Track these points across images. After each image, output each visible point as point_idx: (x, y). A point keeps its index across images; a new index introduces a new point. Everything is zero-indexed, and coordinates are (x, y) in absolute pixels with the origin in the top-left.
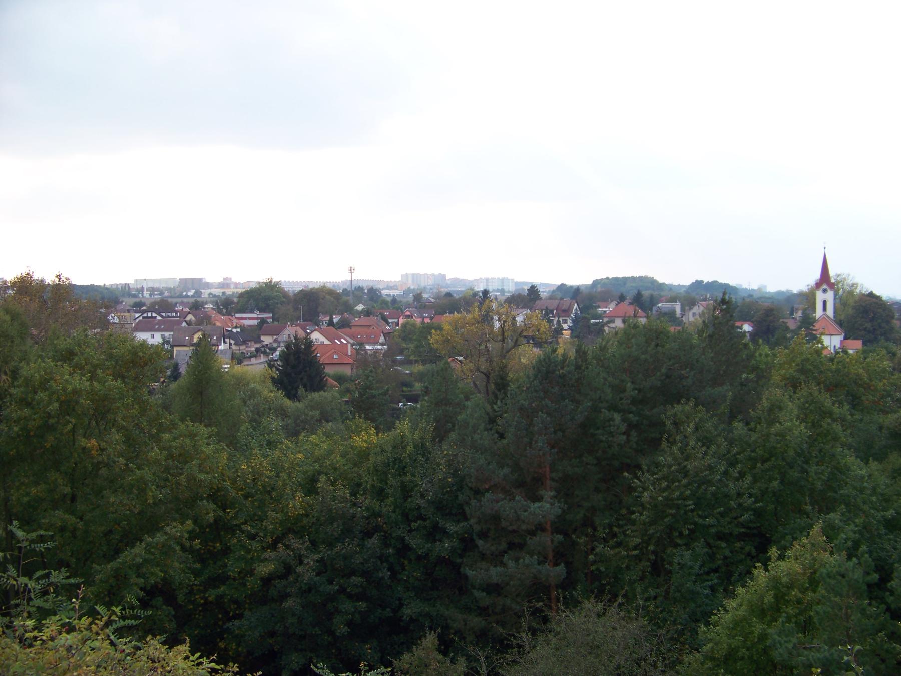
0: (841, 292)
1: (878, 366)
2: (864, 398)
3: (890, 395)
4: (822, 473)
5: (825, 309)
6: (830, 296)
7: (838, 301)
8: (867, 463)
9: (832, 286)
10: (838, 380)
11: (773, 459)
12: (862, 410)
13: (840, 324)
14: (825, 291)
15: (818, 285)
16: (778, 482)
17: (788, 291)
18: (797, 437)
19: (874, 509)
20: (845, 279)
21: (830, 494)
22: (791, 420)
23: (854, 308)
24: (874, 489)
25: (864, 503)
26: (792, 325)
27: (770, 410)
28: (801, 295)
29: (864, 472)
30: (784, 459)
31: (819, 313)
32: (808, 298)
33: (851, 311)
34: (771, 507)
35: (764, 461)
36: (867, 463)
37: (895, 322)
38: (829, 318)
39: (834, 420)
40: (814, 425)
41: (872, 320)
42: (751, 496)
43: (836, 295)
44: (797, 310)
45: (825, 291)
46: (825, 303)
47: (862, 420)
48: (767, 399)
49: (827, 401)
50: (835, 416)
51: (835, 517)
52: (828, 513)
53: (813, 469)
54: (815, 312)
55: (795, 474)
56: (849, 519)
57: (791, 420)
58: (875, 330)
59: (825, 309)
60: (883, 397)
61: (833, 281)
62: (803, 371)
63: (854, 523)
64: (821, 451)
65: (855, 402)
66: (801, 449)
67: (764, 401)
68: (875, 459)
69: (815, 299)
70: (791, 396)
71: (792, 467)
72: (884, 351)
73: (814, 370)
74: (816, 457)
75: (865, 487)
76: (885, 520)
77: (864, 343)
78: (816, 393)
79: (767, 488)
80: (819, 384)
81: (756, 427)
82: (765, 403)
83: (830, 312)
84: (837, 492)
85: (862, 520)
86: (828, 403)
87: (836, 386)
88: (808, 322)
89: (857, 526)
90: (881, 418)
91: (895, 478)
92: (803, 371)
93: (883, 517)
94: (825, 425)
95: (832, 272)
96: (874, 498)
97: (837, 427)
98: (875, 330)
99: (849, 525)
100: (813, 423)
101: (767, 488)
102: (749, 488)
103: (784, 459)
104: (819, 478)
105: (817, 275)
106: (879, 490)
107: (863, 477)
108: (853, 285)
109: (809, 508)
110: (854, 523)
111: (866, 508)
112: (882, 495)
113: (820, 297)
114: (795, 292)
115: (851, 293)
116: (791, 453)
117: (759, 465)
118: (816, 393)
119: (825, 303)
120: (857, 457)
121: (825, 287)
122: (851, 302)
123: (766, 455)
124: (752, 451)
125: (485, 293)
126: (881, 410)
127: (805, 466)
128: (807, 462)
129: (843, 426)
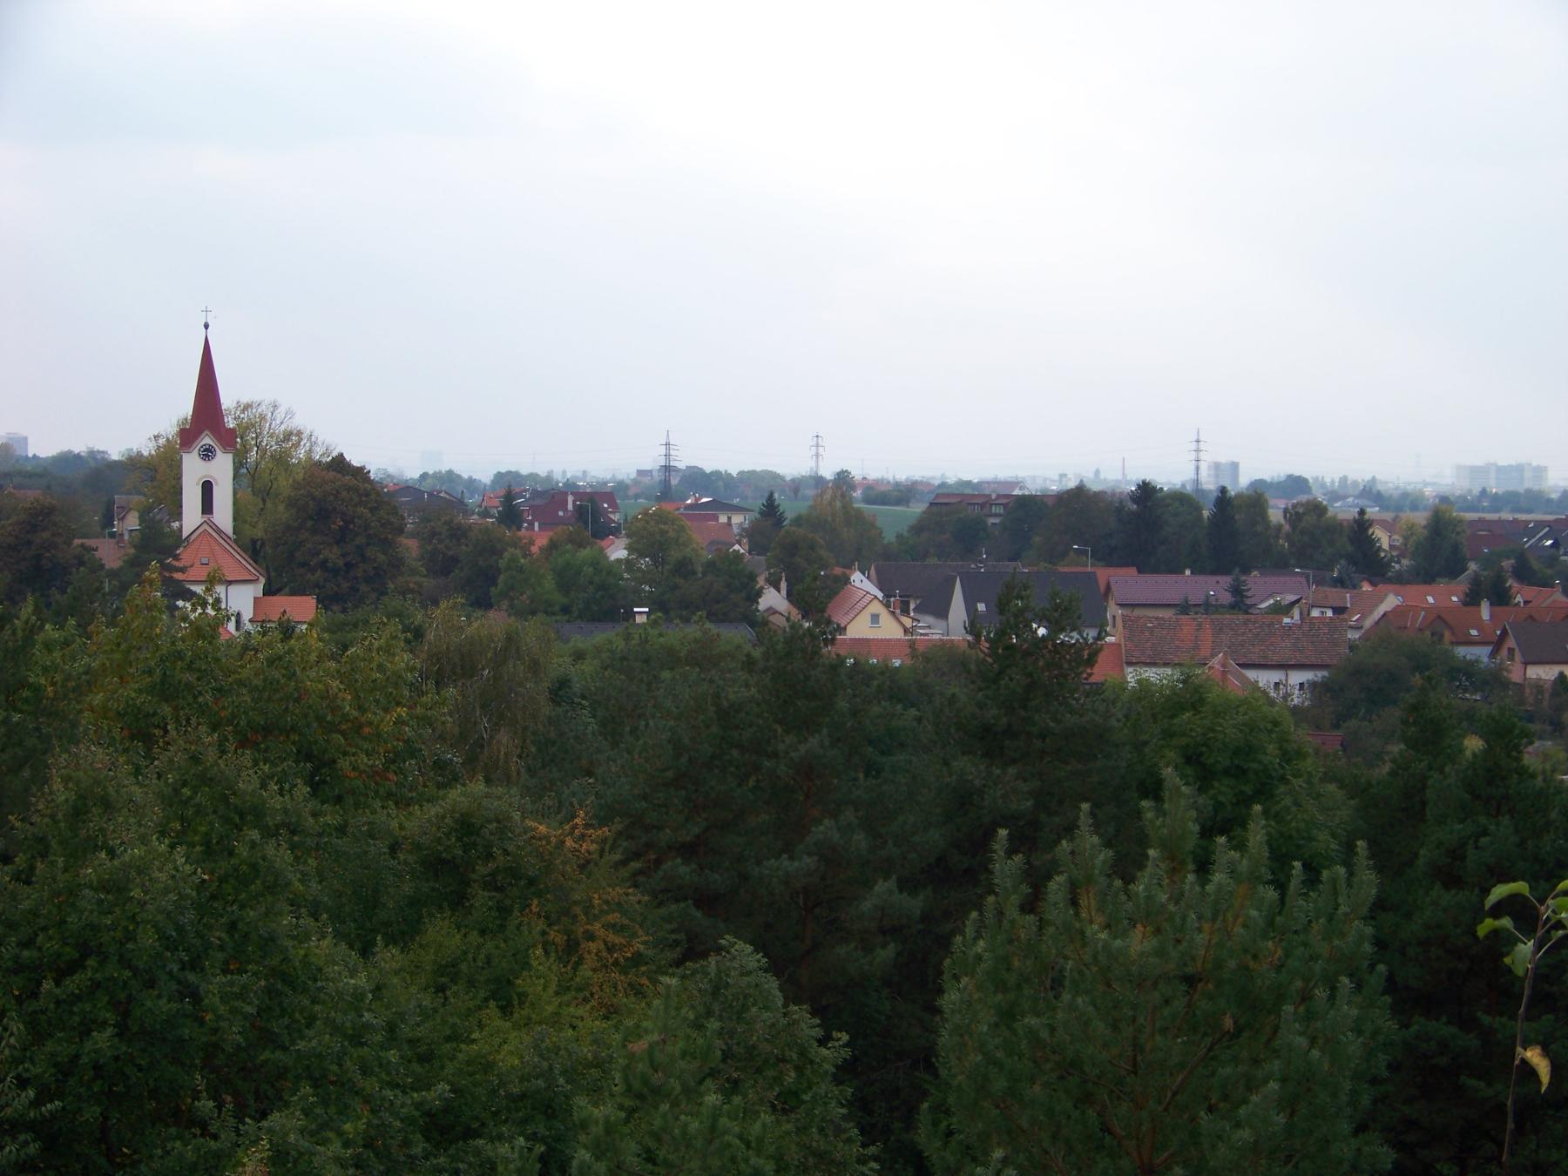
0: (253, 455)
1: (381, 668)
2: (344, 764)
3: (413, 753)
4: (242, 995)
5: (207, 506)
6: (222, 469)
7: (245, 481)
8: (366, 951)
9: (228, 439)
10: (275, 717)
11: (91, 962)
12: (339, 800)
13: (254, 550)
14: (207, 454)
15: (188, 435)
16: (110, 1031)
17: (92, 454)
18: (167, 891)
19: (394, 1085)
20: (263, 417)
21: (267, 1055)
22: (144, 840)
23: (291, 503)
24: (391, 1028)
25: (365, 1071)
26: (110, 555)
27: (78, 813)
28: (134, 464)
29: (361, 981)
30: (125, 962)
31: (191, 516)
32: (155, 476)
33: (282, 513)
34: (91, 1113)
35: (60, 975)
36: (366, 951)
37: (404, 541)
38: (219, 531)
39: (270, 833)
40: (209, 852)
41: (341, 538)
42: (23, 1083)
43: (238, 466)
44: (125, 510)
45: (207, 454)
46: (207, 488)
47: (342, 830)
48: (66, 780)
49: (246, 776)
50: (270, 822)
51: (286, 1123)
52: (264, 1115)
53: (214, 985)
54: (178, 515)
55: (159, 1005)
56: (324, 1126)
57: (144, 840)
58: (348, 565)
59: (207, 506)
60: (395, 759)
61: (231, 423)
62: (166, 690)
63: (340, 1133)
64: (232, 927)
65: (320, 774)
66: (180, 929)
67: (57, 785)
68: (391, 940)
69: (179, 478)
70: (137, 771)
71: (151, 984)
72: (395, 627)
73: (189, 684)
74: (222, 948)
75: (367, 1026)
76: (429, 1114)
77: (325, 602)
78: (211, 755)
79: (77, 1056)
80: (214, 727)
81: (32, 868)
82: (61, 793)
83: (223, 515)
84: (285, 1049)
85: (361, 1126)
86: (247, 783)
87: (267, 730)
88: (159, 542)
89: (346, 1145)
90: (392, 820)
91: (441, 989)
92: (166, 690)
93: (418, 1105)
94: (243, 851)
95: (230, 396)
96: (393, 1055)
97: (279, 854)
98: (348, 565)
99: (325, 1142)
100: (207, 844)
101: (77, 1056)
102: (16, 1062)
103: (125, 962)
104: (234, 1011)
105: (185, 406)
106: (405, 1030)
107: (358, 996)
108: (288, 436)
109: (206, 1105)
110: (340, 1133)
111: (371, 1085)
112: (412, 1042)
113: (193, 469)
114: (115, 455)
115: (281, 460)
116: (148, 939)
117: (47, 985)
118: (211, 755)
119: (207, 488)
120: (337, 935)
121: (207, 440)
122: (284, 485)
123: (71, 953)
124: (28, 943)
125: (1362, 525)
126: (390, 795)
127: (192, 977)
128: (194, 965)
129: (293, 848)
